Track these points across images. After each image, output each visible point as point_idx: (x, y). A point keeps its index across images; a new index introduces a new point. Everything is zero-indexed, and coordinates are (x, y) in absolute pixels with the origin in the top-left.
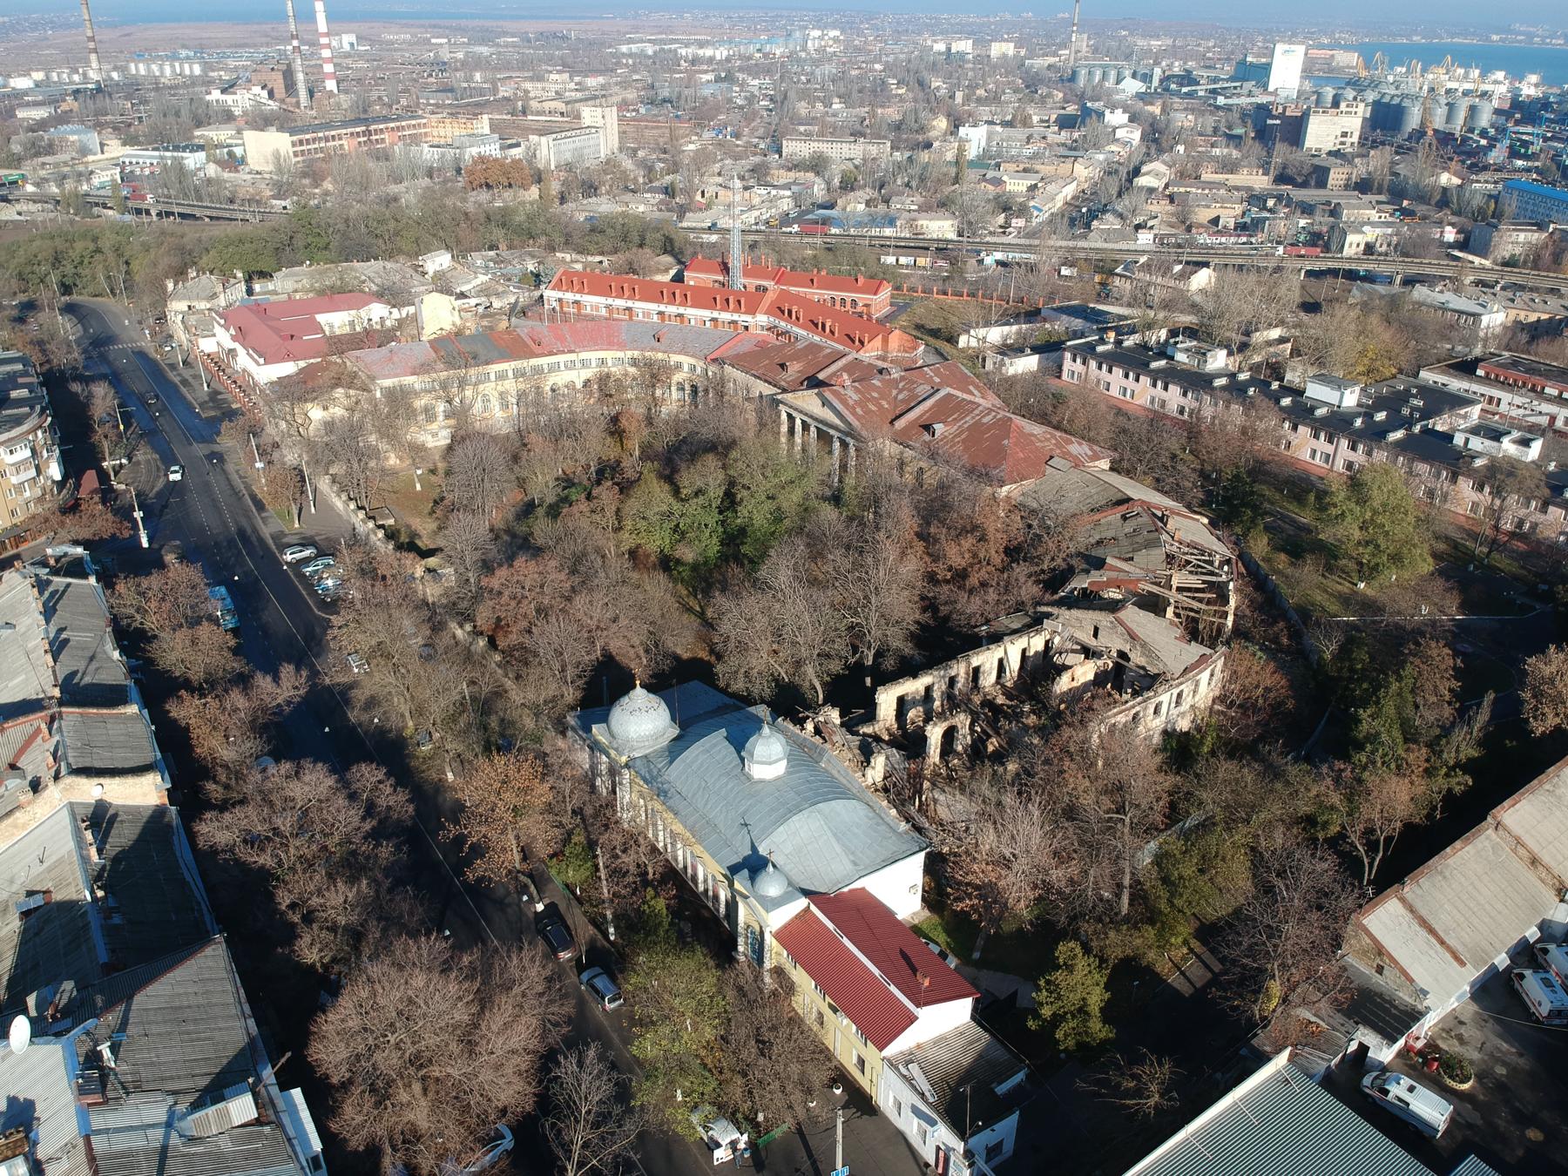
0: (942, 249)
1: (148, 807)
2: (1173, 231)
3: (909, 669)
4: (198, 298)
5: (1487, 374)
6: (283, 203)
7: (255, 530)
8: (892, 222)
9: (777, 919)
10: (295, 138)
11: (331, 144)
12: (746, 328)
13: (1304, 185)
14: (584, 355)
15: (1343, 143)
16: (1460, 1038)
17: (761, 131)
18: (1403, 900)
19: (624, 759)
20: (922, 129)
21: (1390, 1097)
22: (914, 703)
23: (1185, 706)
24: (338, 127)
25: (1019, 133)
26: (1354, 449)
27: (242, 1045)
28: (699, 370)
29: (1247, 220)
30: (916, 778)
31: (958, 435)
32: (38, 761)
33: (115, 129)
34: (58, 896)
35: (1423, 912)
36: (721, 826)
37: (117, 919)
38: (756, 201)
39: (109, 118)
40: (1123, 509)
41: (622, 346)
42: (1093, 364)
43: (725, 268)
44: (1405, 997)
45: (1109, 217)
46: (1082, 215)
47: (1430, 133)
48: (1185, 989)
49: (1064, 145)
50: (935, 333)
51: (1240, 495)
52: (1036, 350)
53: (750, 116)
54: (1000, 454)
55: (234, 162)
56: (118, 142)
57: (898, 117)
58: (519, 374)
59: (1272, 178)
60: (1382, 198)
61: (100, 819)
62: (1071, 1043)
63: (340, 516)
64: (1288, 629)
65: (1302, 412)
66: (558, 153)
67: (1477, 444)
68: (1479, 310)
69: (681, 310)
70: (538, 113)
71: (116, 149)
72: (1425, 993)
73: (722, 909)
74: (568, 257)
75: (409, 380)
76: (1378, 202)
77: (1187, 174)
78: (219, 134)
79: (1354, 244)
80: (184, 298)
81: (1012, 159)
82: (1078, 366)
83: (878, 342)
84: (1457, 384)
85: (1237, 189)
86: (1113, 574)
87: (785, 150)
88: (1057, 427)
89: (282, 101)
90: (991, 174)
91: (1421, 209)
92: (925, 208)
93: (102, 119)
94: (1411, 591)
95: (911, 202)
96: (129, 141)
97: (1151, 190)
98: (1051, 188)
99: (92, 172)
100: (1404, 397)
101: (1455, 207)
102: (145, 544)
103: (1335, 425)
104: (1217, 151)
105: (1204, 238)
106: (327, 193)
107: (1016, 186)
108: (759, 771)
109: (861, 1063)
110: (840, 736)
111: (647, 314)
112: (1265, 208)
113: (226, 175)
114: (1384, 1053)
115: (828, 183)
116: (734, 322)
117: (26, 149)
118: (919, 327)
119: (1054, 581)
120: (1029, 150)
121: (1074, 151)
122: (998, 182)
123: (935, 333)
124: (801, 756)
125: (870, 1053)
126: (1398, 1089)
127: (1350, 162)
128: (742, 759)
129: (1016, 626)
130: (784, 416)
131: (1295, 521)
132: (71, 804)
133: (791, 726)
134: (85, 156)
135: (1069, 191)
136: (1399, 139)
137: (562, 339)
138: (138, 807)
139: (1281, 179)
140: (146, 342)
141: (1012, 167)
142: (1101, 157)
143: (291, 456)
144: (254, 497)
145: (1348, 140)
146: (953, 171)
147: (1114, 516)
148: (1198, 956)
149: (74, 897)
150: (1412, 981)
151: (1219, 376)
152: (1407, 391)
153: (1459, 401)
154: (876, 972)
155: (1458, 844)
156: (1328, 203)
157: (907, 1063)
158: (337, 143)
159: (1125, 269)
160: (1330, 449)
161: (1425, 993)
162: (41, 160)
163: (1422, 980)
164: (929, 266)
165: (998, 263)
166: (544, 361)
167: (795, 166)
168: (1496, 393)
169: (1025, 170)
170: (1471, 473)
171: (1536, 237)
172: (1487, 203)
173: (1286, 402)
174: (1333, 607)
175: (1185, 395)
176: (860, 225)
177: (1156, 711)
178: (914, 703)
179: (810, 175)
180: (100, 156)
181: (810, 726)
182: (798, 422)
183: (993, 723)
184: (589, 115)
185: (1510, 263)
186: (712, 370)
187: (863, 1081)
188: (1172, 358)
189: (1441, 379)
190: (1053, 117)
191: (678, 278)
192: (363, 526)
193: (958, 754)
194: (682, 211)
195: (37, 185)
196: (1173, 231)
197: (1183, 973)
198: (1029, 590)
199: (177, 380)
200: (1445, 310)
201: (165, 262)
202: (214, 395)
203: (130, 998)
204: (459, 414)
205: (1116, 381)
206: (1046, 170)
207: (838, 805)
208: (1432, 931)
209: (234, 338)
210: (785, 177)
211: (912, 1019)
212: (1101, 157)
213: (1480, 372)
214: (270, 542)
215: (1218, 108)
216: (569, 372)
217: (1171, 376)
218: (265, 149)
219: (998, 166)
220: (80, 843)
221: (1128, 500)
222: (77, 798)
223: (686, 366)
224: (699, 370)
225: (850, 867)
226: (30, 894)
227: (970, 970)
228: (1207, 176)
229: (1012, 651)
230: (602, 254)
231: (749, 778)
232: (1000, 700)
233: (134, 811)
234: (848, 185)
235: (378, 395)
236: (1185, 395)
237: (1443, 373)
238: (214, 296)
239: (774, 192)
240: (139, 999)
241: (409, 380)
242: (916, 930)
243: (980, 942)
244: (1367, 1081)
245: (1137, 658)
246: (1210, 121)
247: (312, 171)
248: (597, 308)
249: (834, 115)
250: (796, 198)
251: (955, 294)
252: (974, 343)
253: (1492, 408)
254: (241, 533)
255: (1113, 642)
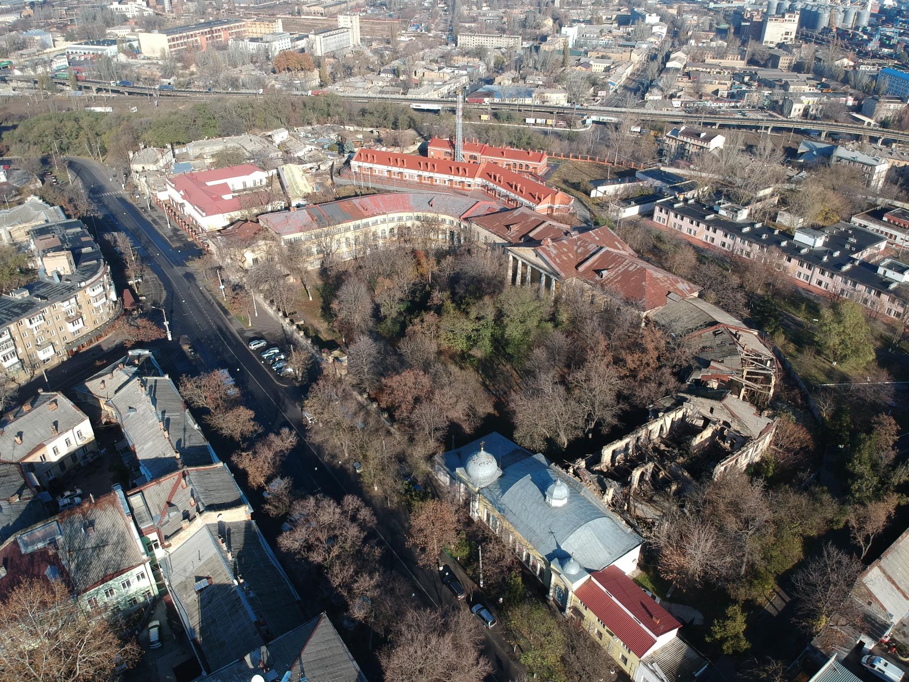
0: (560, 113)
1: (241, 522)
2: (692, 99)
3: (617, 434)
4: (148, 162)
5: (889, 220)
6: (169, 81)
7: (227, 328)
8: (529, 94)
9: (575, 586)
10: (170, 37)
11: (190, 40)
12: (469, 186)
13: (765, 66)
14: (391, 216)
15: (786, 39)
16: (904, 633)
17: (442, 26)
18: (880, 567)
19: (477, 489)
20: (538, 26)
21: (876, 669)
22: (620, 452)
23: (759, 450)
24: (194, 29)
25: (595, 28)
26: (823, 273)
27: (356, 677)
28: (455, 224)
29: (735, 91)
30: (626, 497)
31: (615, 278)
32: (184, 500)
33: (57, 28)
34: (216, 581)
35: (889, 573)
36: (538, 531)
37: (252, 595)
38: (447, 78)
39: (53, 21)
40: (713, 328)
41: (411, 210)
42: (672, 214)
43: (452, 146)
44: (881, 617)
45: (655, 90)
46: (639, 87)
47: (835, 30)
48: (774, 612)
49: (622, 37)
50: (576, 186)
51: (769, 309)
52: (638, 202)
53: (433, 16)
54: (641, 291)
55: (133, 52)
56: (63, 38)
57: (522, 16)
58: (357, 227)
59: (746, 61)
60: (810, 76)
61: (223, 532)
62: (730, 651)
63: (272, 318)
64: (801, 393)
65: (794, 251)
66: (326, 45)
67: (891, 274)
68: (874, 162)
69: (431, 174)
70: (308, 14)
71: (63, 44)
72: (891, 616)
73: (538, 573)
74: (352, 129)
75: (298, 235)
76: (808, 79)
77: (697, 59)
78: (121, 32)
79: (797, 110)
80: (140, 163)
81: (594, 49)
82: (663, 215)
83: (549, 198)
84: (872, 226)
85: (726, 68)
86: (714, 371)
87: (459, 42)
88: (669, 270)
89: (155, 8)
90: (583, 60)
91: (833, 84)
92: (548, 85)
93: (49, 21)
94: (862, 371)
95: (538, 79)
96: (69, 38)
97: (677, 70)
98: (619, 69)
99: (52, 61)
100: (844, 236)
101: (852, 83)
102: (170, 338)
103: (812, 259)
104: (713, 44)
105: (711, 104)
106: (192, 74)
107: (598, 67)
108: (555, 503)
109: (625, 660)
110: (588, 476)
111: (411, 176)
112: (743, 82)
113: (131, 60)
114: (870, 645)
115: (487, 65)
116: (463, 182)
117: (11, 46)
118: (565, 182)
119: (682, 374)
120: (604, 40)
121: (629, 43)
122: (588, 65)
123: (576, 186)
124: (575, 492)
125: (632, 657)
126: (880, 665)
127: (791, 52)
128: (545, 496)
129: (668, 405)
130: (511, 258)
131: (794, 320)
132: (207, 525)
133: (560, 469)
134: (45, 49)
135: (629, 71)
136: (816, 34)
137: (377, 205)
138: (237, 523)
139: (751, 62)
140: (123, 191)
141: (594, 54)
142: (645, 46)
143: (234, 278)
144: (220, 305)
145: (789, 37)
146: (561, 58)
147: (709, 332)
148: (778, 593)
149: (226, 582)
150: (885, 610)
151: (745, 225)
152: (846, 231)
153: (874, 239)
154: (632, 616)
155: (904, 534)
156: (780, 81)
157: (652, 663)
158: (194, 39)
159: (672, 133)
160: (809, 273)
161: (891, 616)
162: (20, 52)
163: (890, 610)
164: (554, 124)
165: (594, 122)
166: (370, 220)
167: (467, 53)
168: (894, 233)
169: (603, 57)
170: (889, 292)
171: (900, 106)
172: (871, 82)
173: (784, 244)
174: (822, 378)
175: (726, 236)
176: (511, 96)
177: (747, 456)
178: (620, 452)
179: (477, 60)
180: (53, 49)
181: (571, 470)
182: (520, 263)
183: (661, 462)
184: (342, 21)
185: (884, 124)
186: (464, 224)
187: (626, 669)
188: (717, 212)
189: (864, 222)
190: (614, 17)
191: (423, 151)
192: (290, 328)
193: (646, 482)
194: (406, 86)
195: (21, 70)
196: (692, 99)
197: (771, 603)
198: (672, 382)
199: (149, 219)
200: (854, 162)
201: (125, 139)
202: (175, 230)
203: (300, 655)
204: (326, 253)
205: (686, 225)
206: (615, 56)
207: (598, 522)
208: (893, 583)
209: (183, 197)
210: (461, 61)
211: (654, 642)
212: (645, 46)
213: (885, 219)
214: (238, 335)
215: (710, 10)
216: (383, 225)
217: (718, 224)
218: (154, 44)
219: (586, 53)
220: (219, 548)
221: (715, 323)
222: (209, 522)
223: (448, 221)
224: (455, 224)
225: (608, 555)
226: (198, 579)
227: (665, 603)
228: (709, 60)
229: (667, 421)
230: (372, 126)
231: (549, 506)
232: (663, 447)
233: (236, 524)
234: (500, 68)
235: (283, 244)
236: (726, 236)
237: (864, 218)
238: (157, 161)
239: (456, 72)
240: (303, 656)
241: (298, 235)
242: (635, 581)
243: (671, 590)
244: (864, 660)
245: (735, 426)
246: (706, 20)
247: (182, 58)
248: (382, 172)
249: (484, 15)
250: (470, 75)
251: (582, 158)
252: (600, 195)
253: (892, 240)
254: (220, 329)
255: (721, 416)
